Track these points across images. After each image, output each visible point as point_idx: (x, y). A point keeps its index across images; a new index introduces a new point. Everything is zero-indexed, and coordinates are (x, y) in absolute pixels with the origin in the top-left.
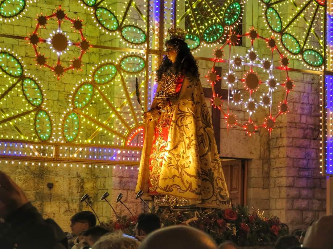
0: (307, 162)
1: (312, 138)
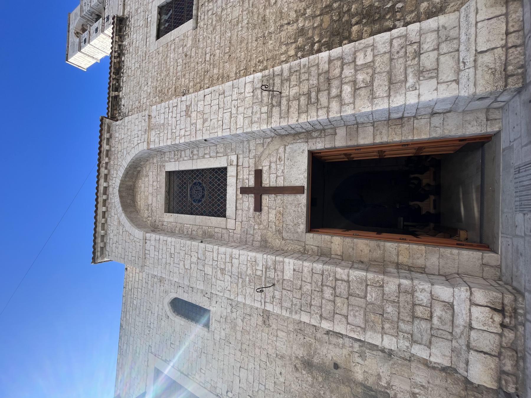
0: (302, 96)
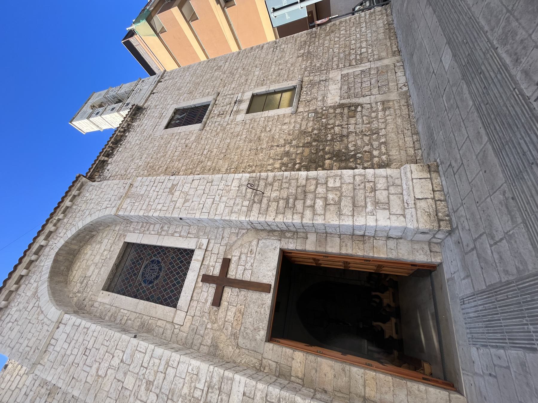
1: (262, 195)
